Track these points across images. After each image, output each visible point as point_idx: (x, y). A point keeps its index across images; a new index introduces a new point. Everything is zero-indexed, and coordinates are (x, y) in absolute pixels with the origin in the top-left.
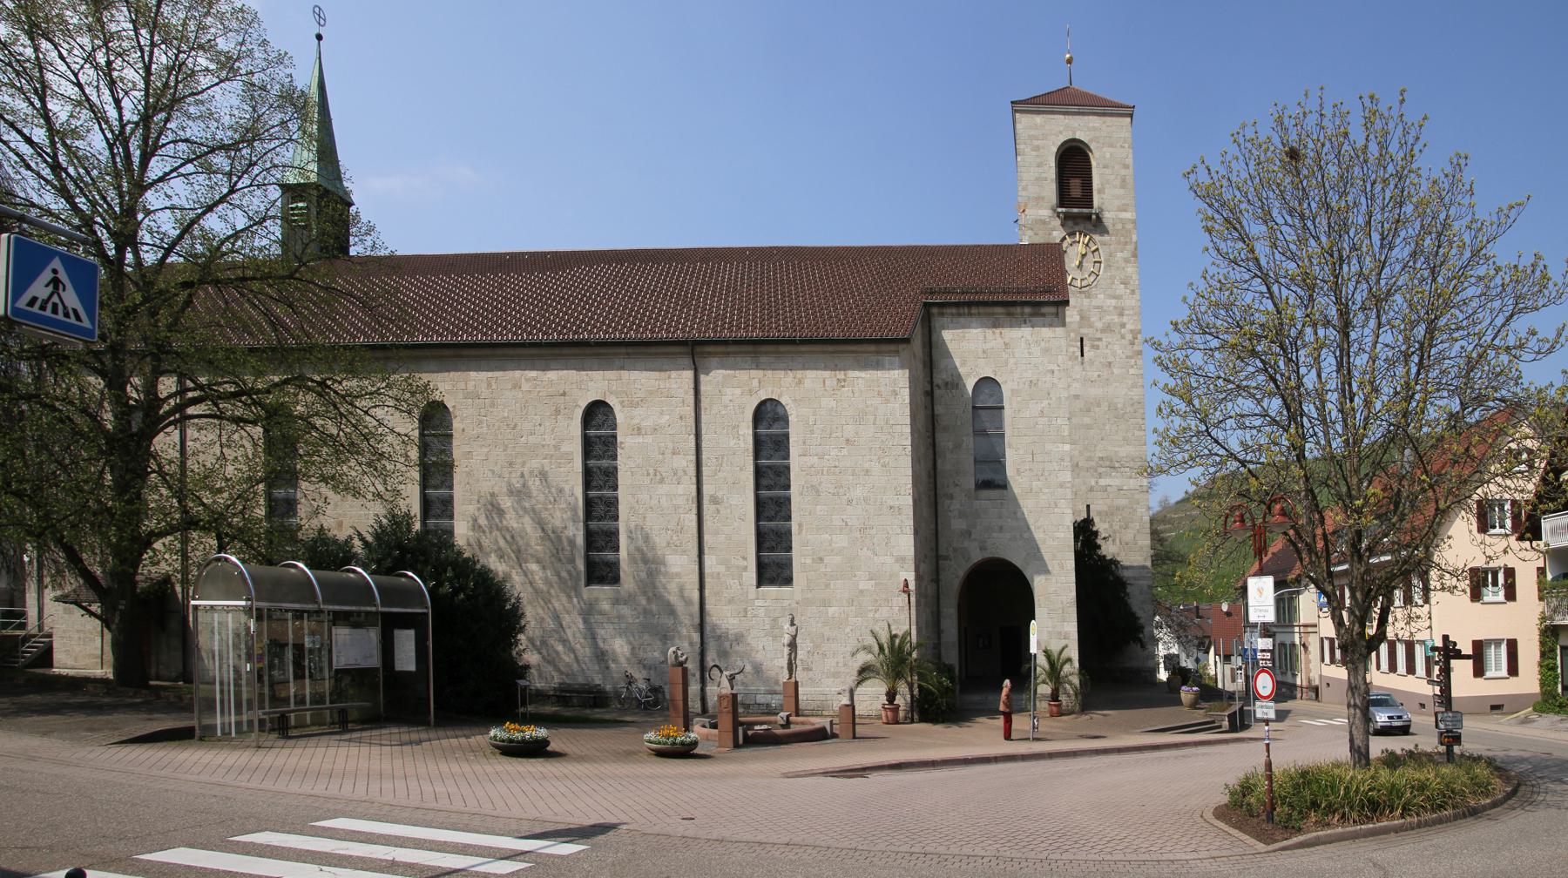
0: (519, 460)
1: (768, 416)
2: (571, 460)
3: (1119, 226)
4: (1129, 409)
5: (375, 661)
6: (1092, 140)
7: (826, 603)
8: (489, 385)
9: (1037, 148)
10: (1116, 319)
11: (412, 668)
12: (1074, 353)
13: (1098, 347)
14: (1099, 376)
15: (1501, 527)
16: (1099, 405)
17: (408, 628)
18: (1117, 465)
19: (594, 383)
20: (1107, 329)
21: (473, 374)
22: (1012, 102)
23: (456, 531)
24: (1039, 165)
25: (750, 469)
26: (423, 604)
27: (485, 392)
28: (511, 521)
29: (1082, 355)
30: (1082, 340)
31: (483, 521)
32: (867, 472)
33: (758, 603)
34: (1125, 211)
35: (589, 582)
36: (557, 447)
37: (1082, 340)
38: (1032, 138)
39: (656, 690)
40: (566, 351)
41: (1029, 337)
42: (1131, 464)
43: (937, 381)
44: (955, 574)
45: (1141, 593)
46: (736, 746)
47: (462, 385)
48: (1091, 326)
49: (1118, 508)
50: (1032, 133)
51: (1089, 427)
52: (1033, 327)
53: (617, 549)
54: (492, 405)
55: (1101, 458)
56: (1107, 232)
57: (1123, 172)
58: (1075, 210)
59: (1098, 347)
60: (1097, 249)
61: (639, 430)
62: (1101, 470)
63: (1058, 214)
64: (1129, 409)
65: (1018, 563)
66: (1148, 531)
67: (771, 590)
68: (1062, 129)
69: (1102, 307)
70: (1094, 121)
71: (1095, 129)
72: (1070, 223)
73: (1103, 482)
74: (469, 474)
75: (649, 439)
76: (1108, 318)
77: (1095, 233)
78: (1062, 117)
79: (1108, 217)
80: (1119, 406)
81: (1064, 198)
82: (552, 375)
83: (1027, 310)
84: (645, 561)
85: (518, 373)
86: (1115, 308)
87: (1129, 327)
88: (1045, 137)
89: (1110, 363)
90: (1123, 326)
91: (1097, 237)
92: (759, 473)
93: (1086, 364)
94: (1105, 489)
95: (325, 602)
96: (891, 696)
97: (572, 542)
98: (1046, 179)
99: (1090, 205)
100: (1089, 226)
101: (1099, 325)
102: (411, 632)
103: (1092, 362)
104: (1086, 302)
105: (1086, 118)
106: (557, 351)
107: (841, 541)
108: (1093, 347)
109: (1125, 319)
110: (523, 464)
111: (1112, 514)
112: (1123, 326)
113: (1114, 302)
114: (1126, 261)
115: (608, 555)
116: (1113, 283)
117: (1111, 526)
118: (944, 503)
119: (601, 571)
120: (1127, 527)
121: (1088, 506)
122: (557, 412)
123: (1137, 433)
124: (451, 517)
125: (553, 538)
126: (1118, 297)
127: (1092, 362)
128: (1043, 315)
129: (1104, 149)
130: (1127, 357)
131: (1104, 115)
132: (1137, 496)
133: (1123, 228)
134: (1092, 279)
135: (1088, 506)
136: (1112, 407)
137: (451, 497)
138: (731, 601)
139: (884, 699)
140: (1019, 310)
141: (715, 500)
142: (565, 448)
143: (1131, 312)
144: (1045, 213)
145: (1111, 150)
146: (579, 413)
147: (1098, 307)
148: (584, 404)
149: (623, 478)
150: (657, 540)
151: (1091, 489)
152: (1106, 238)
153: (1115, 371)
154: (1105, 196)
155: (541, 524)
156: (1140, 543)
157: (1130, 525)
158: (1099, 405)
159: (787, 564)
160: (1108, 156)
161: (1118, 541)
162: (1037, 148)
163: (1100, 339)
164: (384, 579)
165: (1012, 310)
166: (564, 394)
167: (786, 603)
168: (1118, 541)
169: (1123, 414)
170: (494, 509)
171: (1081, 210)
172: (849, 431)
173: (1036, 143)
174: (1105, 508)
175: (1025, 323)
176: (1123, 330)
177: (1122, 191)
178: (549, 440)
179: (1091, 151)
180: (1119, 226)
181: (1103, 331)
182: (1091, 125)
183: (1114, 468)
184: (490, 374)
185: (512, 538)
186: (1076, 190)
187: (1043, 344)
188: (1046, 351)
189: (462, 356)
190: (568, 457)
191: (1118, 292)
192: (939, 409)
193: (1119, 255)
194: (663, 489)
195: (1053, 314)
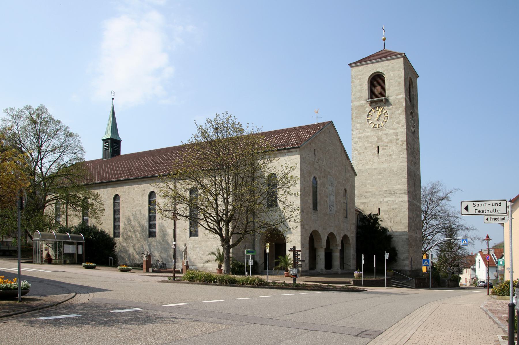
0: (134, 207)
2: (146, 207)
5: (75, 252)
6: (384, 71)
7: (207, 241)
8: (128, 189)
10: (394, 137)
11: (81, 253)
12: (374, 152)
14: (386, 160)
16: (385, 171)
17: (80, 245)
18: (393, 193)
20: (391, 141)
21: (125, 187)
22: (349, 64)
23: (121, 225)
25: (147, 208)
26: (83, 240)
27: (127, 191)
28: (133, 223)
29: (378, 153)
30: (378, 147)
31: (126, 223)
33: (189, 241)
35: (150, 237)
36: (143, 203)
37: (378, 147)
38: (357, 76)
39: (164, 264)
40: (145, 179)
41: (287, 159)
45: (402, 241)
47: (122, 190)
48: (382, 141)
49: (393, 209)
50: (357, 74)
51: (380, 180)
52: (288, 156)
53: (156, 228)
54: (129, 194)
56: (391, 105)
57: (399, 80)
58: (375, 99)
60: (386, 112)
63: (368, 102)
66: (407, 217)
67: (193, 238)
68: (371, 69)
69: (388, 134)
70: (386, 63)
71: (386, 66)
72: (374, 104)
73: (386, 200)
74: (123, 211)
76: (390, 138)
77: (385, 106)
78: (371, 65)
79: (391, 99)
80: (395, 170)
81: (372, 94)
82: (142, 186)
83: (286, 151)
84: (163, 231)
85: (134, 186)
86: (394, 133)
87: (400, 139)
88: (363, 74)
89: (391, 154)
91: (386, 108)
94: (387, 202)
95: (57, 239)
96: (220, 266)
97: (146, 228)
98: (363, 90)
99: (384, 95)
100: (382, 104)
101: (386, 140)
102: (81, 246)
103: (382, 155)
105: (382, 63)
106: (142, 180)
108: (383, 149)
110: (135, 208)
111: (390, 211)
112: (398, 139)
113: (393, 131)
115: (154, 230)
116: (393, 124)
117: (389, 216)
119: (152, 234)
121: (379, 209)
122: (143, 195)
124: (120, 222)
125: (142, 227)
127: (382, 155)
128: (292, 152)
129: (391, 73)
130: (399, 151)
131: (391, 60)
133: (399, 101)
134: (384, 123)
135: (379, 209)
137: (120, 217)
138: (182, 241)
139: (218, 268)
140: (282, 151)
142: (145, 203)
143: (402, 134)
144: (363, 102)
145: (394, 72)
148: (149, 192)
150: (165, 226)
152: (391, 107)
154: (390, 91)
155: (139, 223)
156: (403, 222)
157: (398, 215)
160: (392, 75)
161: (392, 222)
163: (387, 146)
164: (41, 233)
165: (280, 152)
166: (144, 190)
167: (196, 242)
168: (392, 222)
169: (397, 173)
170: (129, 220)
171: (377, 99)
174: (387, 209)
175: (286, 155)
176: (397, 141)
179: (384, 75)
182: (384, 65)
184: (128, 187)
185: (133, 227)
186: (378, 90)
187: (291, 161)
189: (122, 183)
190: (145, 206)
191: (395, 127)
195: (295, 151)
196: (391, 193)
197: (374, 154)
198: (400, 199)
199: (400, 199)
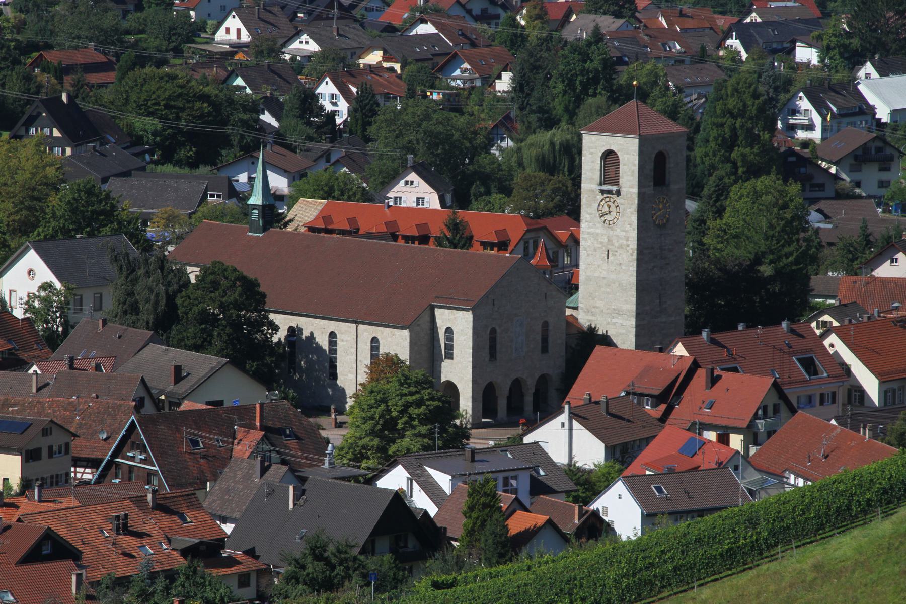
1: (375, 340)
3: (629, 196)
9: (592, 153)
13: (615, 255)
16: (614, 283)
17: (232, 532)
20: (621, 247)
42: (628, 313)
46: (336, 427)
49: (620, 334)
51: (608, 293)
55: (614, 309)
59: (615, 255)
61: (343, 341)
62: (613, 315)
65: (455, 383)
73: (614, 320)
90: (628, 246)
94: (615, 324)
101: (617, 244)
103: (612, 262)
104: (611, 232)
108: (614, 255)
109: (629, 243)
112: (628, 246)
113: (624, 233)
127: (612, 262)
136: (620, 285)
141: (360, 361)
146: (328, 334)
149: (338, 352)
151: (608, 323)
153: (623, 268)
158: (614, 283)
159: (452, 354)
162: (592, 153)
173: (592, 150)
181: (618, 247)
183: (619, 314)
186: (611, 169)
194: (348, 357)
196: (618, 312)
198: (628, 323)
199: (628, 323)
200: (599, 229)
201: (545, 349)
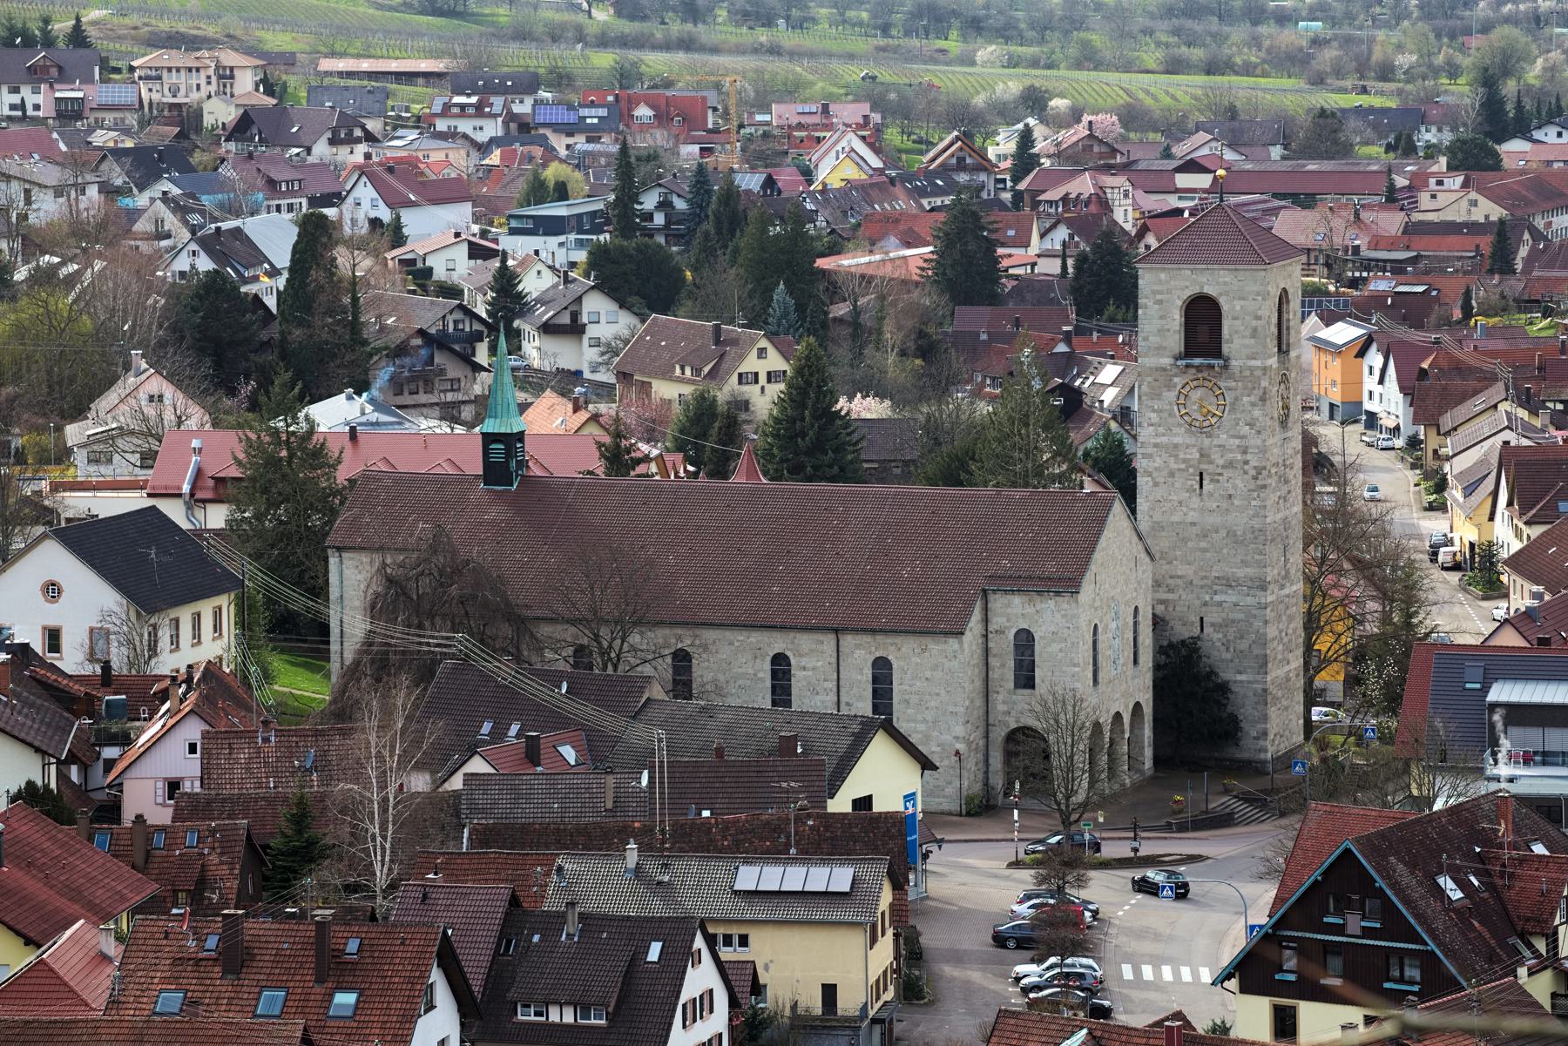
4: (1250, 536)
6: (1221, 294)
9: (1160, 302)
10: (1239, 457)
13: (1218, 481)
15: (715, 936)
16: (1217, 532)
19: (778, 643)
20: (1230, 465)
24: (1162, 318)
30: (1201, 474)
32: (938, 694)
34: (1255, 359)
36: (755, 675)
37: (1201, 474)
38: (1155, 293)
43: (990, 629)
44: (999, 734)
49: (1233, 621)
50: (1156, 288)
51: (1205, 550)
55: (1218, 578)
62: (1215, 587)
64: (1250, 536)
71: (1225, 283)
73: (1217, 598)
75: (810, 673)
87: (1253, 463)
90: (1246, 462)
92: (875, 691)
93: (1205, 497)
94: (1220, 604)
101: (1221, 462)
104: (1207, 441)
107: (921, 727)
109: (1249, 457)
113: (1237, 442)
114: (1253, 404)
118: (993, 696)
120: (1242, 637)
121: (1202, 619)
123: (1257, 557)
126: (1242, 437)
127: (1211, 495)
132: (1254, 612)
135: (1202, 619)
136: (1231, 533)
142: (761, 675)
145: (1242, 302)
146: (769, 659)
147: (1220, 446)
148: (772, 654)
158: (1217, 532)
160: (1238, 308)
162: (1160, 302)
163: (1221, 474)
172: (928, 674)
173: (1159, 297)
174: (1220, 620)
176: (1246, 467)
177: (1253, 341)
178: (751, 671)
180: (1247, 373)
188: (1064, 616)
190: (762, 680)
192: (991, 645)
193: (1245, 399)
194: (819, 698)
197: (1191, 490)
200: (1180, 437)
201: (1136, 662)
